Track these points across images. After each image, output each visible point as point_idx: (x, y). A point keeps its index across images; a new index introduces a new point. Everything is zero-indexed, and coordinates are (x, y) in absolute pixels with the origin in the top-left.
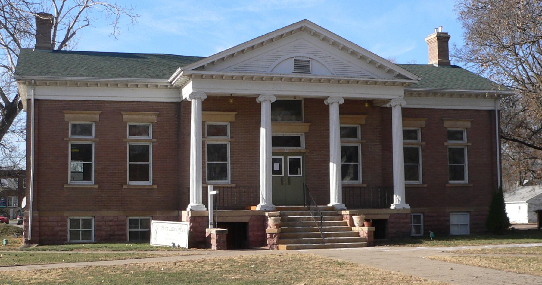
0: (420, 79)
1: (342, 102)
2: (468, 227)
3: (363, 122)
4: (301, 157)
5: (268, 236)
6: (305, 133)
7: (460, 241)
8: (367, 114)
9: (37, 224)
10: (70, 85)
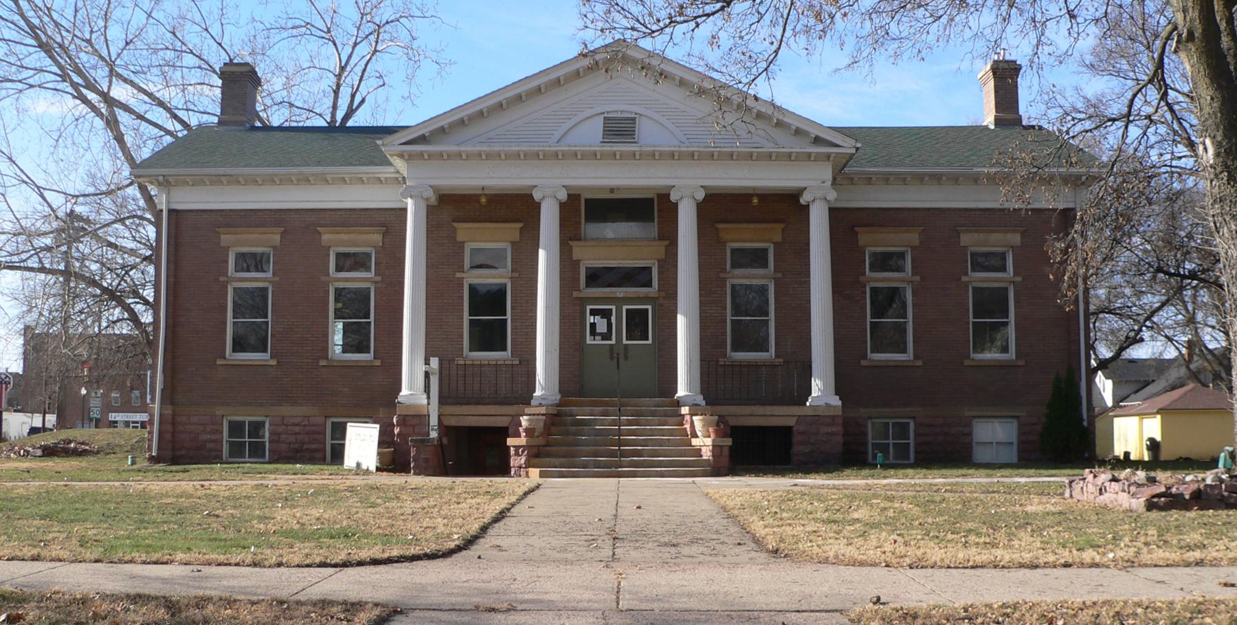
0: (859, 145)
1: (701, 195)
2: (1015, 447)
3: (778, 238)
4: (649, 307)
5: (512, 451)
6: (659, 261)
7: (892, 472)
8: (753, 221)
9: (169, 428)
10: (229, 183)
